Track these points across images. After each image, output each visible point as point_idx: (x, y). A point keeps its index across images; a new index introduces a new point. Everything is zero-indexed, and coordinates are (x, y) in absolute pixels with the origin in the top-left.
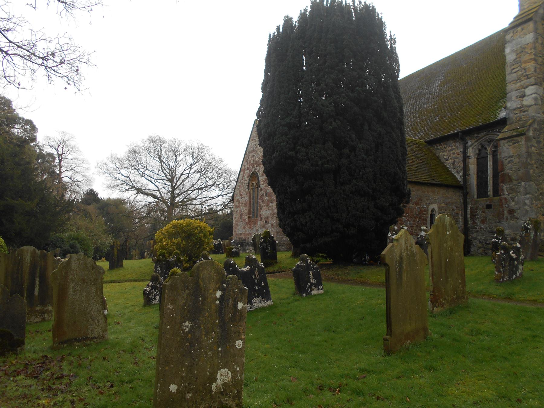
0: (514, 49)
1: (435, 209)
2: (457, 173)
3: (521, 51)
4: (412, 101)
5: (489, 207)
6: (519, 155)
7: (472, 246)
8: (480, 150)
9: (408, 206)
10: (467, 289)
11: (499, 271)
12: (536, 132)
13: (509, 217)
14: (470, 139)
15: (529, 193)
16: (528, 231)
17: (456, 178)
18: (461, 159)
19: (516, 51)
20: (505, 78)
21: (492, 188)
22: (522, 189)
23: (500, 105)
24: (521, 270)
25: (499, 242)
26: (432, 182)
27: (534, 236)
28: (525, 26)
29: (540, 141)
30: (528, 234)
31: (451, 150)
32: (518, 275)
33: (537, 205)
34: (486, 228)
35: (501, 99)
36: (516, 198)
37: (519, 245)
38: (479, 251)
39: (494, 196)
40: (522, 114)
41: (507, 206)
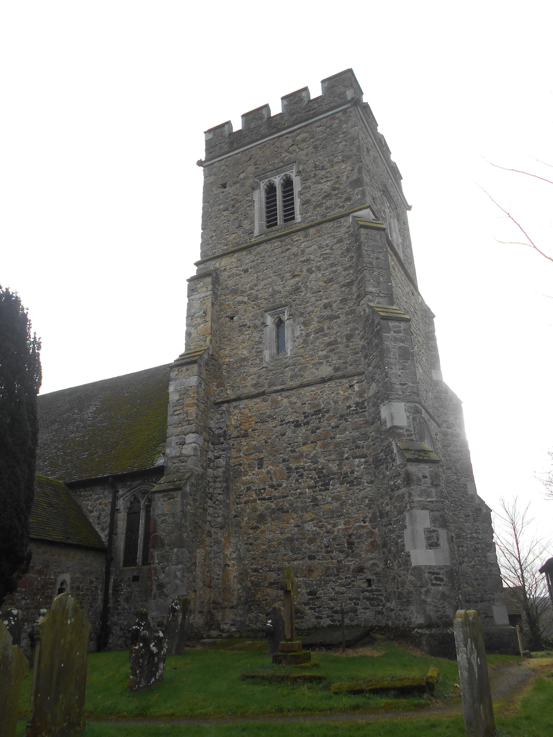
0: (177, 388)
1: (67, 581)
2: (101, 531)
3: (184, 392)
4: (56, 426)
5: (136, 579)
6: (173, 514)
7: (110, 635)
8: (132, 503)
9: (28, 576)
10: (88, 706)
11: (135, 674)
12: (193, 488)
13: (157, 594)
14: (122, 487)
15: (181, 563)
16: (176, 613)
17: (99, 537)
18: (109, 512)
19: (180, 391)
20: (166, 419)
21: (141, 553)
22: (174, 557)
23: (159, 449)
24: (161, 669)
25: (141, 630)
26: (66, 541)
27: (181, 621)
28: (190, 367)
29: (197, 499)
30: (175, 617)
31: (97, 499)
32: (157, 678)
33: (188, 578)
34: (130, 609)
35: (160, 443)
36: (167, 568)
37: (162, 634)
38: (119, 642)
39: (143, 564)
40: (180, 464)
41: (156, 578)
